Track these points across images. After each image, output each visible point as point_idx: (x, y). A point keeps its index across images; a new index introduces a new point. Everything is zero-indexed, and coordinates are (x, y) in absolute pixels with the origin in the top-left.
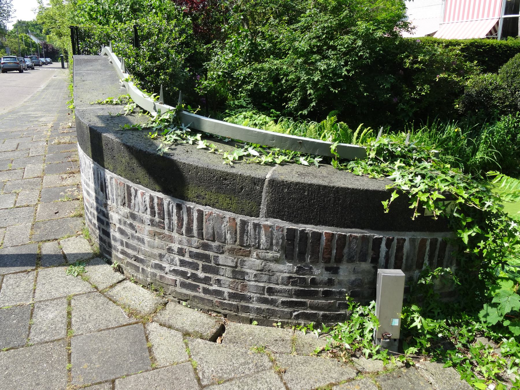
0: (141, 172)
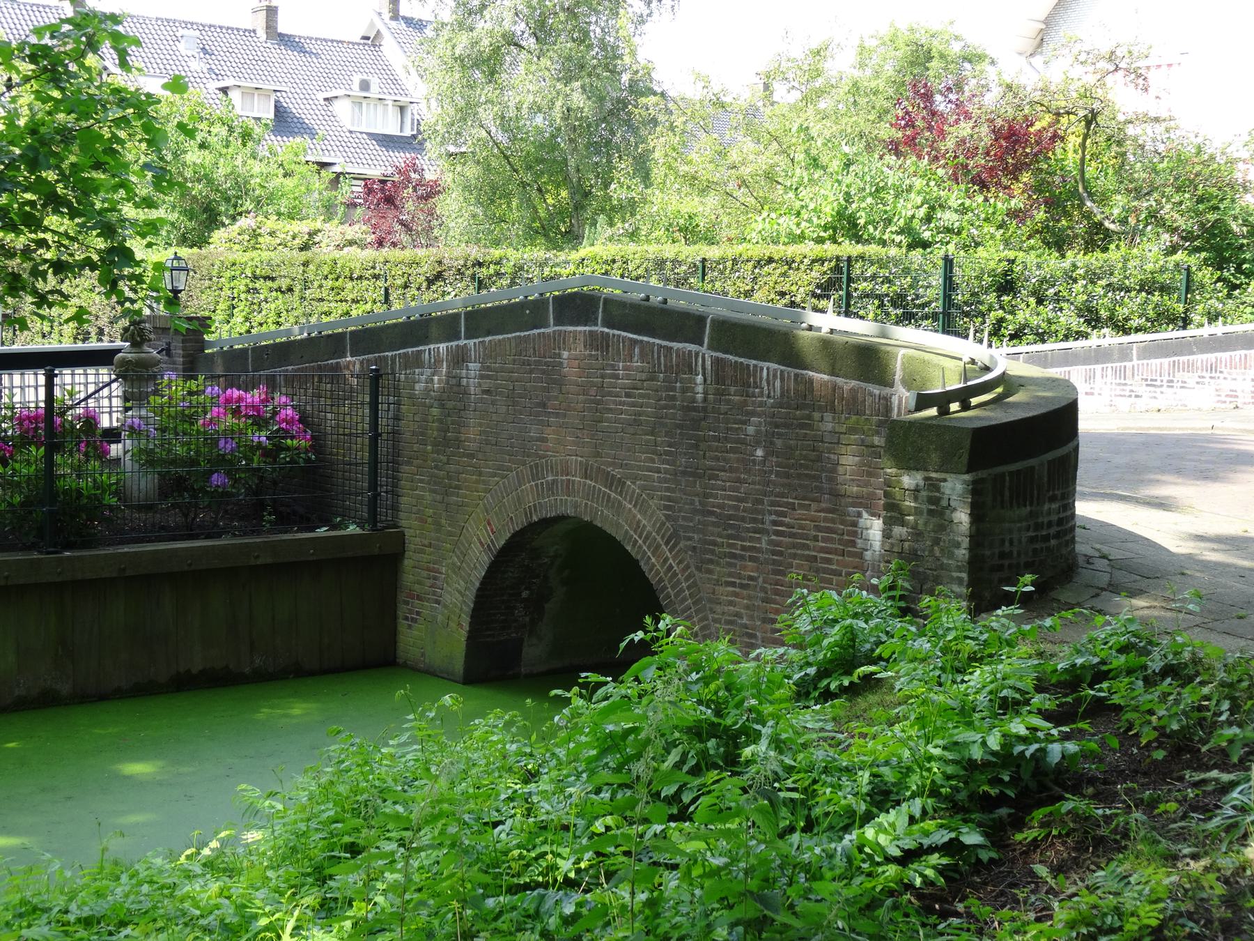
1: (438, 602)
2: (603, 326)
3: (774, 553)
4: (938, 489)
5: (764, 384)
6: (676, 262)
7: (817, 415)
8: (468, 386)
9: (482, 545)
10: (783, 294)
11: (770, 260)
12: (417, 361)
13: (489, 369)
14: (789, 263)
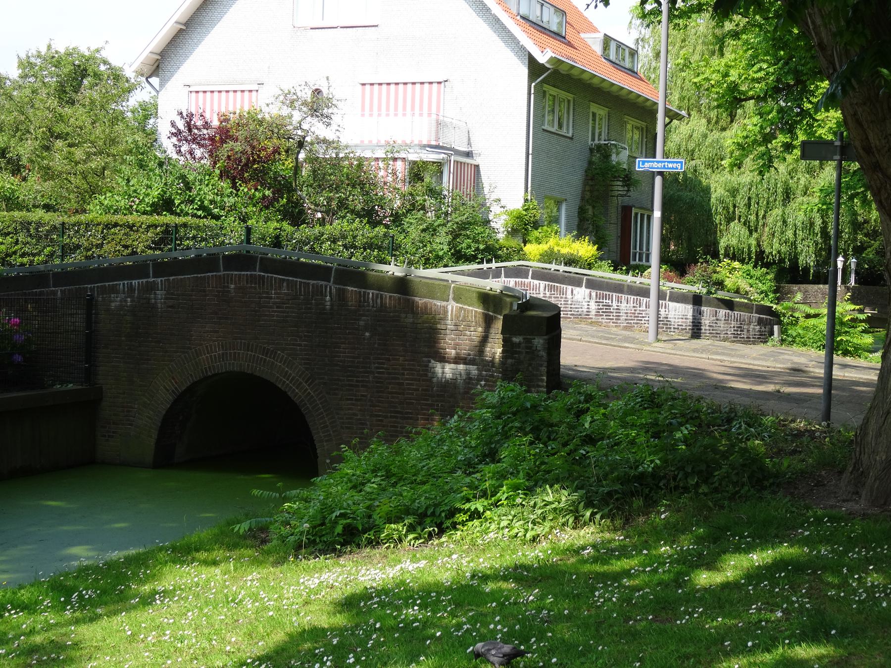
0: (722, 305)
1: (131, 425)
2: (260, 271)
3: (377, 382)
4: (531, 343)
5: (371, 301)
6: (39, 224)
7: (403, 315)
8: (156, 303)
9: (168, 390)
10: (126, 247)
11: (116, 225)
12: (114, 290)
13: (172, 294)
14: (131, 227)
